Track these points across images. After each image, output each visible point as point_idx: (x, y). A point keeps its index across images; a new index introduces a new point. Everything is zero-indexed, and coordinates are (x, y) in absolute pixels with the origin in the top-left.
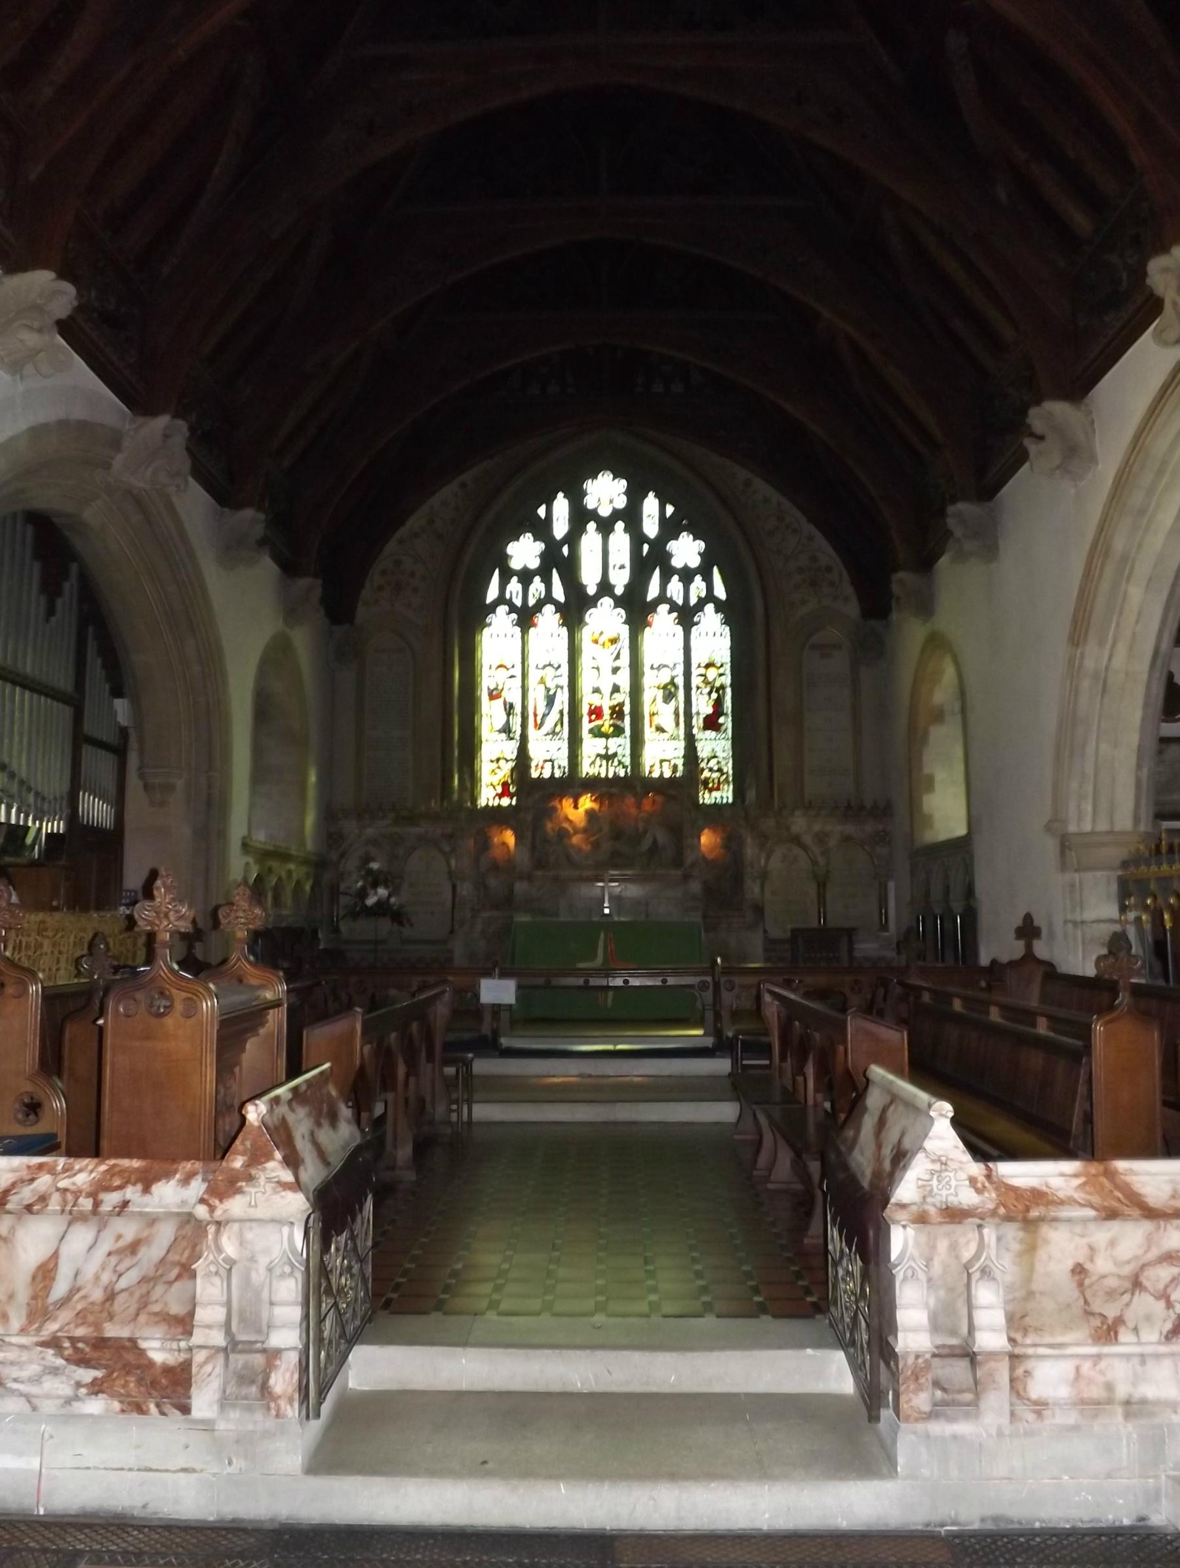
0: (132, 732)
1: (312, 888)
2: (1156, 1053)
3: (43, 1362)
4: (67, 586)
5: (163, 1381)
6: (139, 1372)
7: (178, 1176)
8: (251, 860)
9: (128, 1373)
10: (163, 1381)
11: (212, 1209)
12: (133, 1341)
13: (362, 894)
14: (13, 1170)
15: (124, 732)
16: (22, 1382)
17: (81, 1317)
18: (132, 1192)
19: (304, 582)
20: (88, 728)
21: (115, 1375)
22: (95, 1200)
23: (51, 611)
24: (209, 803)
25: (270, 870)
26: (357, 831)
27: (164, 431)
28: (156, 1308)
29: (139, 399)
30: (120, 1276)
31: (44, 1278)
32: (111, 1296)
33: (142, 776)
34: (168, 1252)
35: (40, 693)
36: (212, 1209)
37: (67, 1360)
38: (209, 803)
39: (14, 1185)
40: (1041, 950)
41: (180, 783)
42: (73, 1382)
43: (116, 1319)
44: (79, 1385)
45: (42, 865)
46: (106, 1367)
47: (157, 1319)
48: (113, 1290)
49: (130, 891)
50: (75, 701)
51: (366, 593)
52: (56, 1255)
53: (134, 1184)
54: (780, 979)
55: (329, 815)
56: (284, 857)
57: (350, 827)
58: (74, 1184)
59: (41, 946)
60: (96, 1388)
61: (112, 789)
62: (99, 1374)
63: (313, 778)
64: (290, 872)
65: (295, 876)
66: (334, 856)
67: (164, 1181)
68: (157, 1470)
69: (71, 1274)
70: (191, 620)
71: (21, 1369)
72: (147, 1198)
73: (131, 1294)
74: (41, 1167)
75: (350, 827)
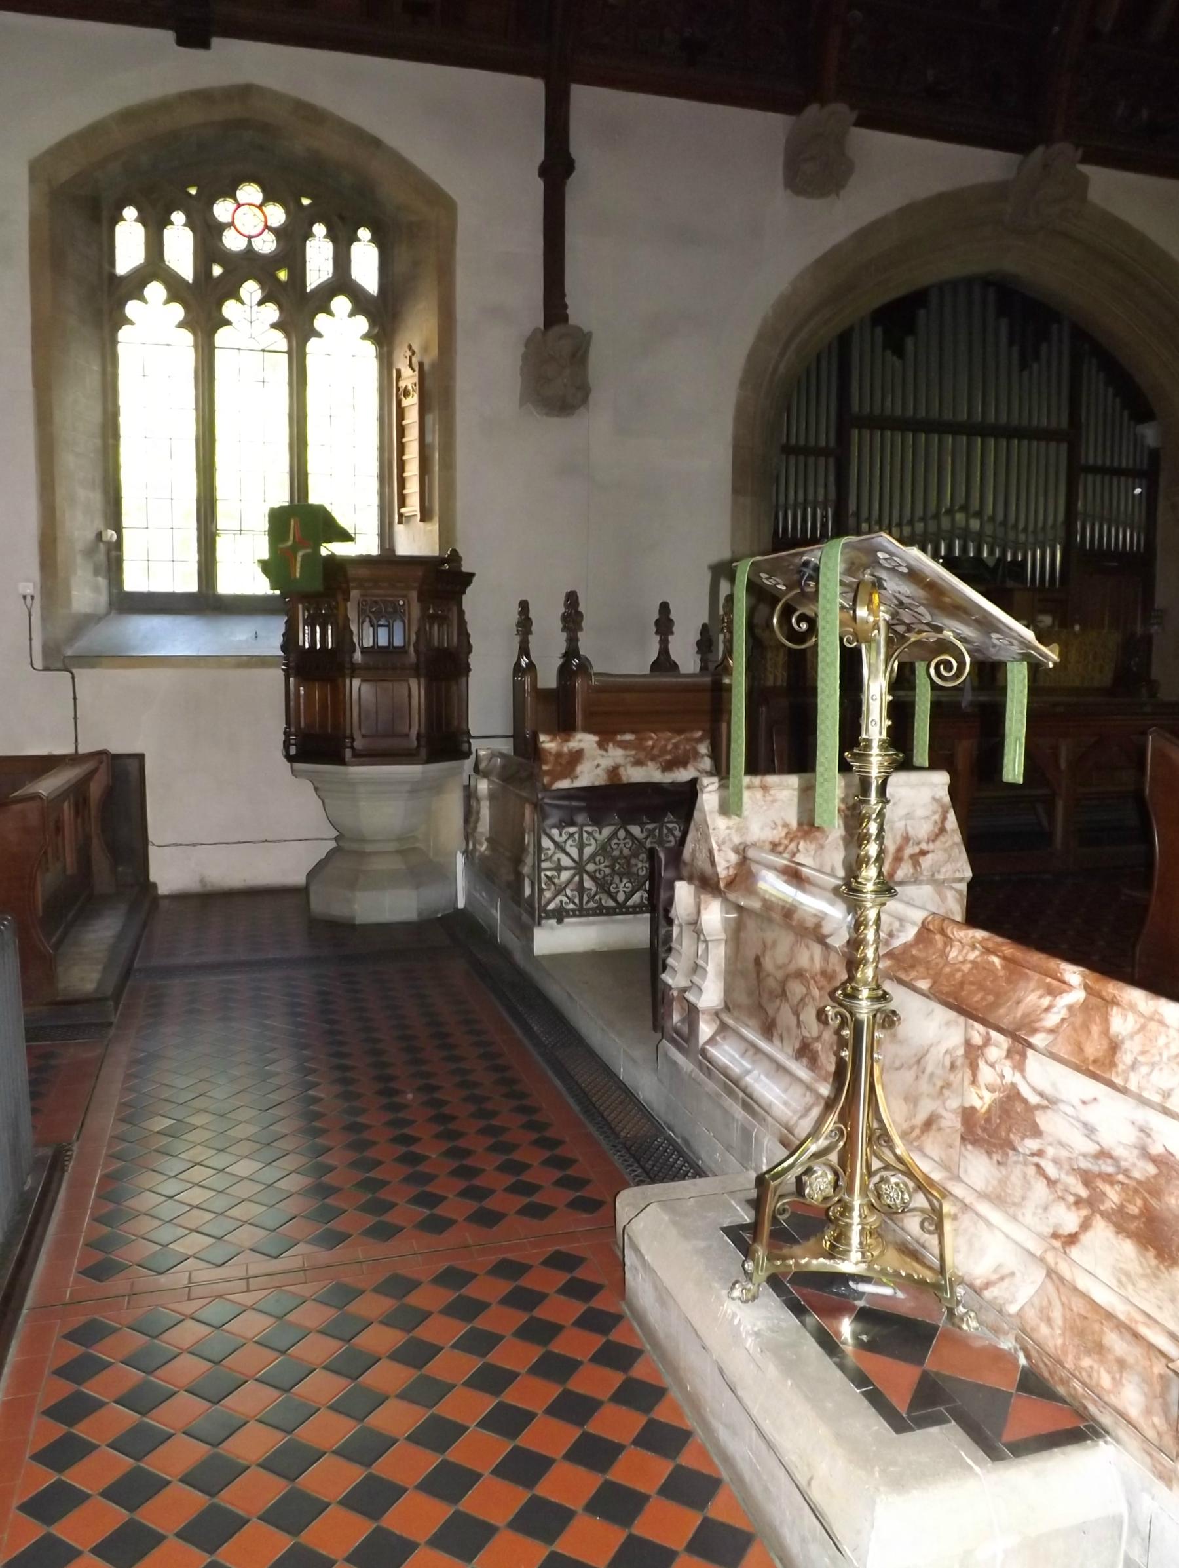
50: (1071, 436)
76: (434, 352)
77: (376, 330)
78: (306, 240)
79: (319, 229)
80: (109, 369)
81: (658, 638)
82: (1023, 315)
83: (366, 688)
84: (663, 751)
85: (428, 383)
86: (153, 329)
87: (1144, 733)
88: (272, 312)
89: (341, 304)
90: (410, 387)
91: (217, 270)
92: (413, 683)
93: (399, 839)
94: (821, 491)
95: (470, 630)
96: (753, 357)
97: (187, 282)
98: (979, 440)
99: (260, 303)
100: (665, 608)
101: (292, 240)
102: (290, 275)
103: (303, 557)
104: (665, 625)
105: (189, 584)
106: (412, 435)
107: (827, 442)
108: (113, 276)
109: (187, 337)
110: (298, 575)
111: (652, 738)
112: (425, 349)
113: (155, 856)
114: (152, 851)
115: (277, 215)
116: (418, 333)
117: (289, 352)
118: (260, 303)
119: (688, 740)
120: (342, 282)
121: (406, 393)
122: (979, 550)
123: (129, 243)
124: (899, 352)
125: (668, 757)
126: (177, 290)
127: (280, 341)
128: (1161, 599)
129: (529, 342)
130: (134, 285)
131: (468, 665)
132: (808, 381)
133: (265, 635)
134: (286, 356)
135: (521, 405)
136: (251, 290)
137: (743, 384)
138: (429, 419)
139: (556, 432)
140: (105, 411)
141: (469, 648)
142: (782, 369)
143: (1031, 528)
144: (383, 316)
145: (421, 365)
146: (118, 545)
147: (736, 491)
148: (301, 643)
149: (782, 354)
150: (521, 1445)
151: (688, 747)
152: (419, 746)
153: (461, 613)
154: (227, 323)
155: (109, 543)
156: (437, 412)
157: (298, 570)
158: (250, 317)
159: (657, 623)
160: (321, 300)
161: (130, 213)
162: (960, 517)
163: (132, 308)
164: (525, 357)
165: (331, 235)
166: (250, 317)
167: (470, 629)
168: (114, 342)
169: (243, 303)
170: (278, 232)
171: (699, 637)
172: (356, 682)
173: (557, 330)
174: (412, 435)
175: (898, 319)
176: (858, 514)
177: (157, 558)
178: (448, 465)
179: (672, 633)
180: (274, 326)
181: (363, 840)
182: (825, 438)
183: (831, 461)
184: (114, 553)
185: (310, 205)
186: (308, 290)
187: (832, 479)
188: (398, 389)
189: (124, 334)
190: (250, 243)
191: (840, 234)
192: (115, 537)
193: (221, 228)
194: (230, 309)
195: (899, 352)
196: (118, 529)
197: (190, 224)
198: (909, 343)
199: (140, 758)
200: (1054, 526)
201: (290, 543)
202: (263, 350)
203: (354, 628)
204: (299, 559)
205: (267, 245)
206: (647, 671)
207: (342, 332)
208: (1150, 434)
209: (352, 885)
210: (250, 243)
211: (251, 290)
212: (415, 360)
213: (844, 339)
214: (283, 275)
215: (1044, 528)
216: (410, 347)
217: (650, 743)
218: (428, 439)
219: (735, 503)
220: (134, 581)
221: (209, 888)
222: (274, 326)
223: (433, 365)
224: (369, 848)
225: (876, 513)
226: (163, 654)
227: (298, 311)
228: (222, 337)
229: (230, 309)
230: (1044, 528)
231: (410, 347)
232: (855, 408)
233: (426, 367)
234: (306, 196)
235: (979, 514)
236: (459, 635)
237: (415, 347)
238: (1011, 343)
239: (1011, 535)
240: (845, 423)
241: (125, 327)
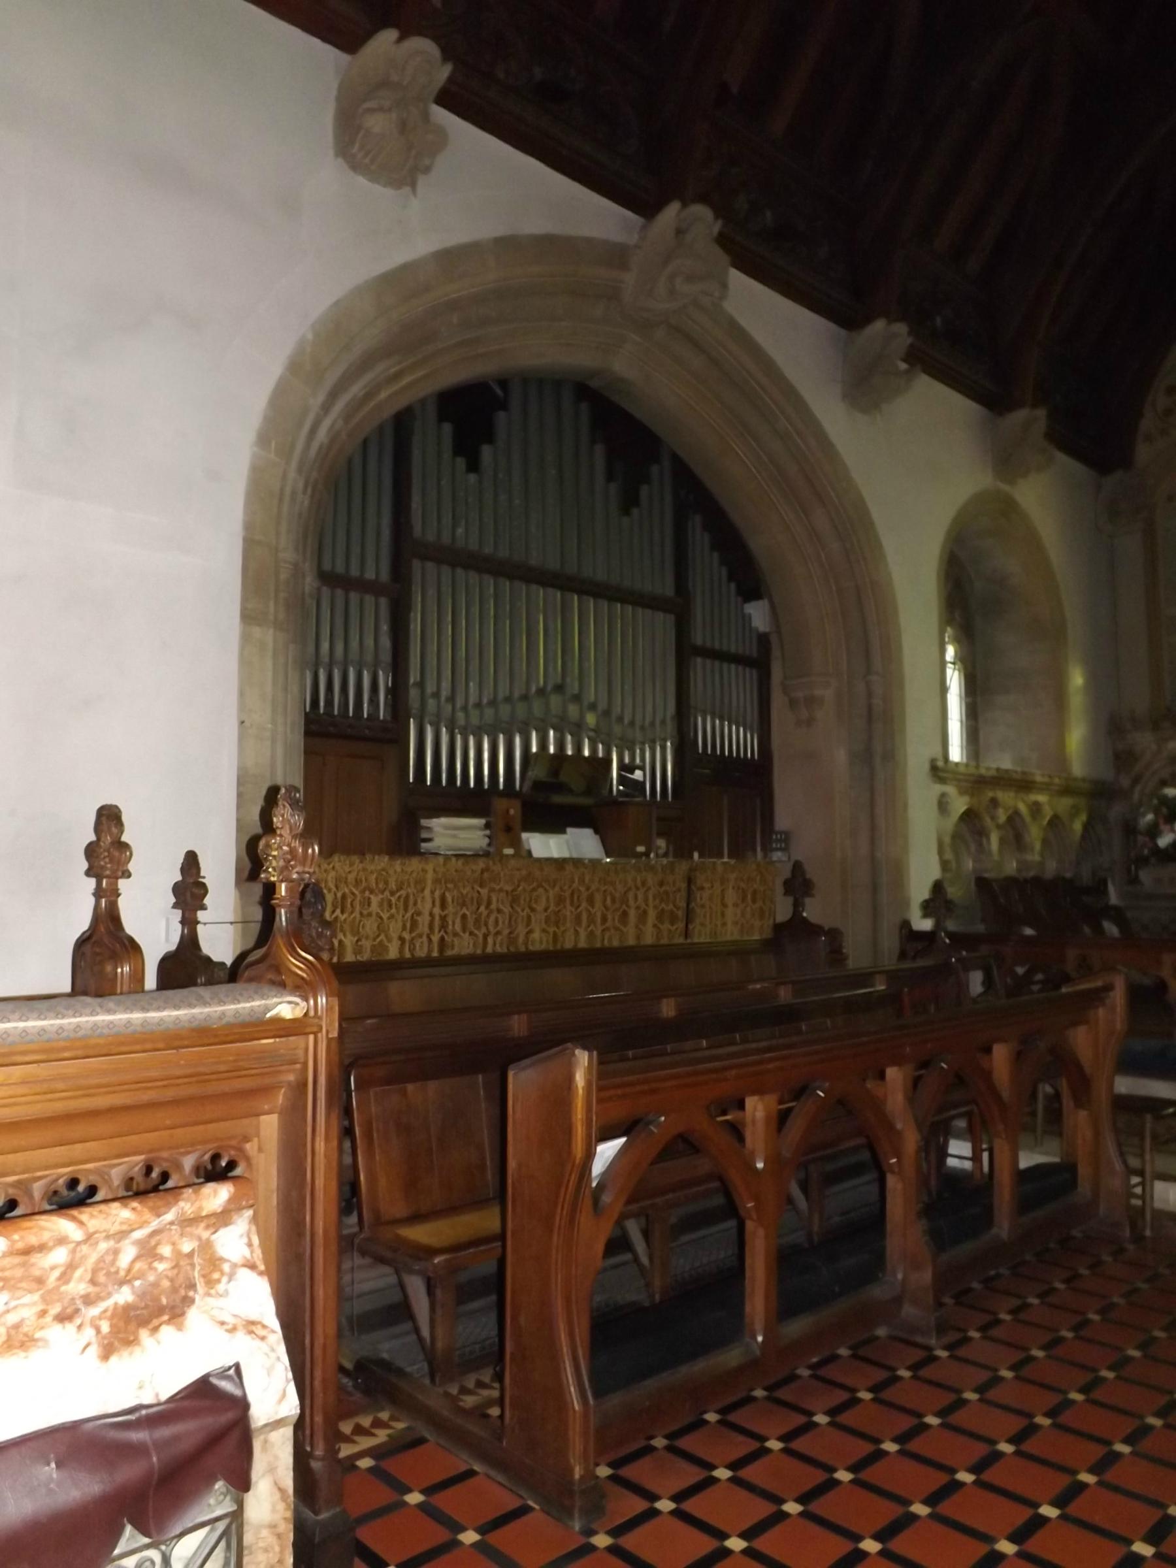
0: (774, 640)
1: (1087, 827)
4: (655, 469)
8: (950, 790)
13: (1153, 832)
15: (763, 640)
19: (1020, 416)
20: (698, 638)
23: (629, 502)
24: (870, 718)
25: (994, 802)
26: (1154, 747)
27: (691, 222)
29: (638, 190)
33: (785, 690)
35: (612, 599)
38: (870, 718)
40: (812, 912)
41: (828, 694)
49: (781, 833)
50: (679, 608)
51: (1147, 423)
55: (1114, 727)
56: (1024, 785)
57: (1144, 741)
59: (381, 904)
61: (752, 714)
63: (1077, 679)
64: (1036, 809)
65: (1048, 813)
66: (1125, 782)
70: (815, 482)
75: (1144, 741)
81: (92, 883)
82: (621, 436)
84: (105, 1276)
87: (988, 1050)
94: (369, 642)
96: (280, 393)
98: (576, 597)
100: (109, 817)
104: (107, 852)
107: (377, 574)
111: (62, 1241)
119: (187, 1222)
122: (578, 748)
124: (474, 466)
125: (125, 1296)
128: (782, 821)
132: (350, 479)
137: (263, 439)
142: (322, 435)
143: (638, 723)
147: (247, 617)
149: (326, 408)
151: (187, 1246)
159: (91, 851)
162: (555, 700)
171: (178, 877)
175: (471, 412)
176: (421, 685)
179: (127, 875)
182: (378, 569)
183: (383, 601)
187: (385, 628)
191: (420, 246)
195: (474, 466)
198: (486, 452)
200: (663, 722)
206: (58, 976)
208: (758, 615)
213: (402, 424)
215: (653, 724)
217: (59, 1256)
219: (245, 638)
225: (446, 686)
230: (653, 724)
232: (417, 530)
235: (577, 698)
238: (610, 477)
239: (617, 730)
240: (404, 548)
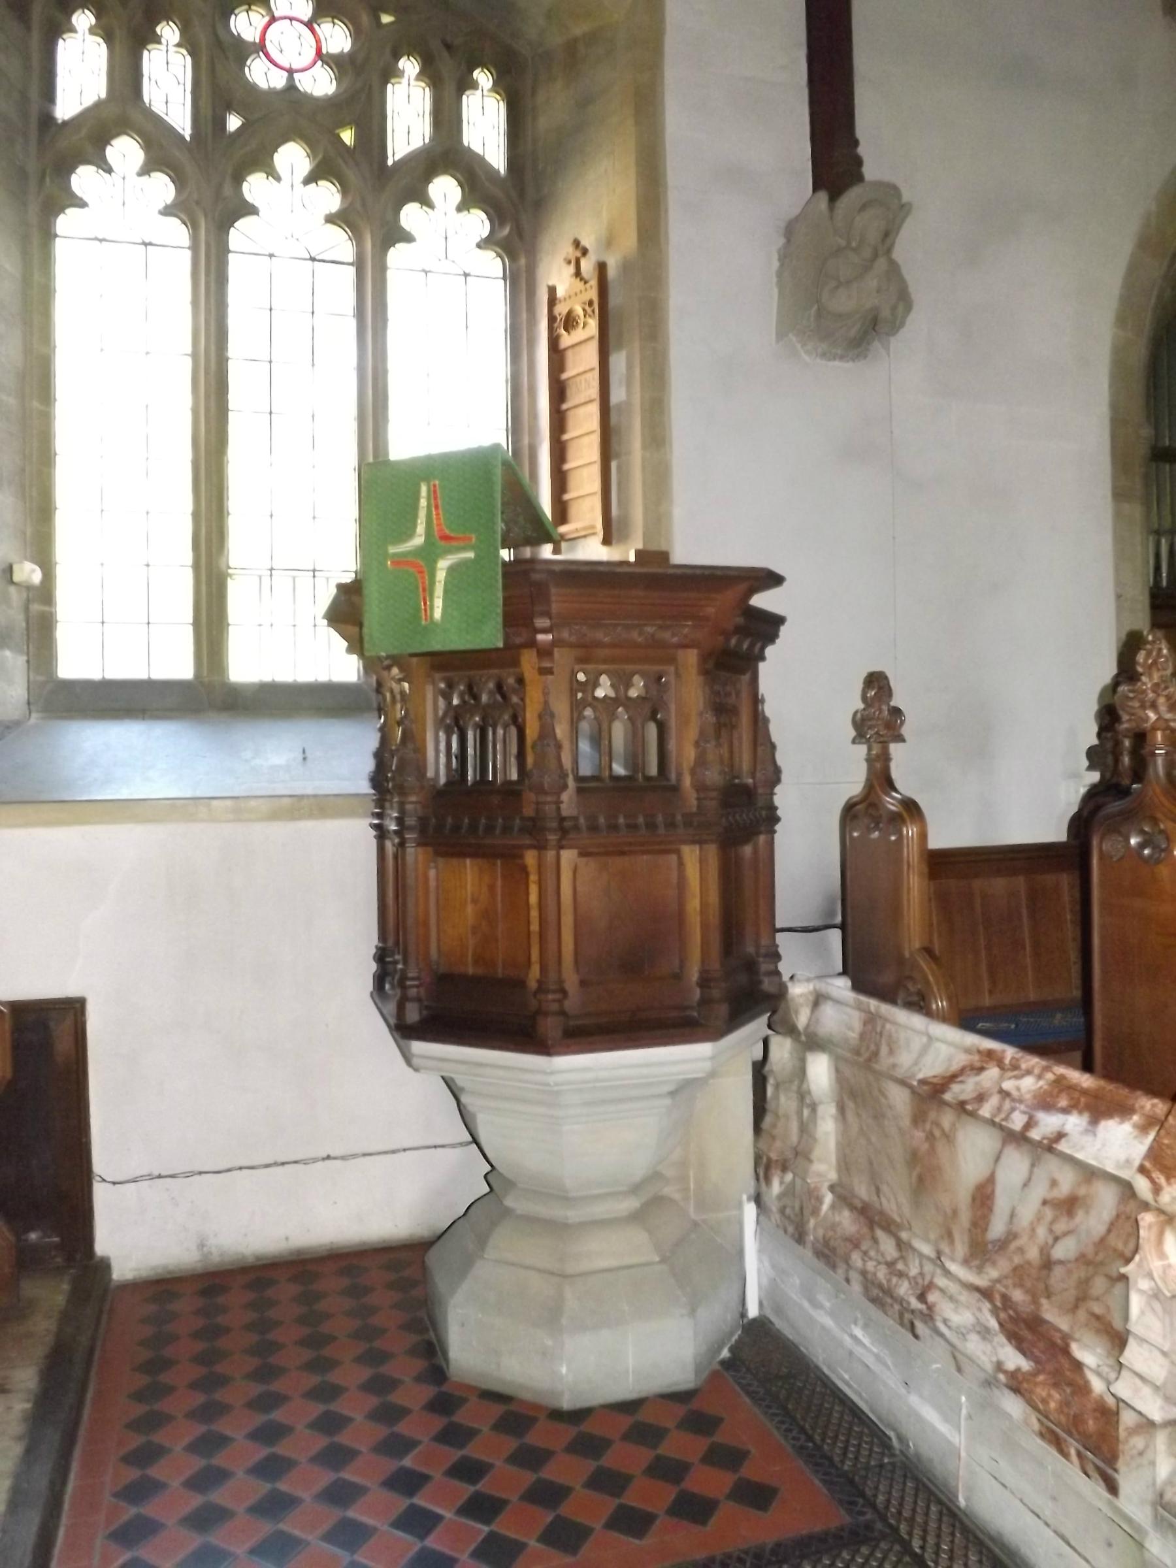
2: (472, 1523)
3: (978, 1314)
5: (1091, 1422)
6: (1068, 1390)
7: (1136, 1118)
9: (1056, 1385)
10: (1091, 1422)
11: (1157, 1190)
12: (1066, 1338)
14: (968, 1051)
16: (949, 1328)
17: (1019, 1273)
18: (1074, 1123)
21: (1041, 1378)
22: (1031, 1118)
28: (1097, 1309)
30: (1056, 1239)
31: (983, 1204)
32: (1048, 1264)
34: (1109, 1231)
36: (1157, 1190)
37: (1001, 1324)
39: (962, 1071)
42: (994, 1359)
43: (1053, 1299)
44: (999, 1367)
45: (571, 682)
46: (1037, 1361)
47: (1096, 1324)
48: (1049, 1256)
52: (991, 1180)
53: (1081, 1112)
54: (715, 965)
58: (1018, 1089)
60: (1017, 1384)
62: (1025, 1365)
67: (1117, 1119)
68: (1079, 1554)
69: (1007, 1212)
71: (956, 1310)
72: (1089, 1139)
73: (1069, 1272)
74: (990, 1055)
76: (629, 241)
77: (506, 231)
78: (386, 82)
79: (409, 66)
80: (37, 277)
83: (589, 867)
85: (614, 300)
86: (119, 211)
88: (328, 196)
89: (445, 189)
90: (579, 311)
91: (234, 123)
92: (691, 854)
93: (635, 1189)
95: (775, 736)
97: (182, 137)
99: (308, 180)
101: (363, 78)
102: (358, 137)
103: (451, 570)
105: (177, 663)
106: (584, 390)
108: (47, 120)
109: (177, 232)
110: (438, 614)
112: (609, 242)
113: (105, 1202)
114: (100, 1193)
115: (337, 37)
116: (591, 215)
117: (359, 264)
118: (308, 180)
120: (446, 152)
121: (570, 322)
123: (81, 68)
126: (161, 151)
127: (340, 244)
129: (790, 230)
130: (92, 137)
131: (773, 808)
133: (345, 758)
134: (352, 270)
135: (781, 335)
136: (293, 158)
138: (618, 361)
139: (839, 389)
140: (27, 350)
141: (776, 776)
144: (515, 208)
145: (602, 267)
146: (45, 593)
147: (1119, 495)
148: (430, 774)
150: (465, 1485)
152: (705, 1002)
153: (756, 700)
154: (252, 210)
155: (29, 588)
156: (637, 345)
157: (438, 603)
158: (290, 201)
160: (412, 179)
161: (83, 20)
163: (84, 179)
164: (784, 256)
165: (430, 74)
166: (290, 201)
167: (776, 733)
168: (48, 235)
169: (278, 179)
170: (337, 63)
172: (568, 856)
173: (852, 196)
174: (584, 390)
177: (117, 609)
178: (657, 438)
180: (331, 219)
181: (565, 1198)
184: (36, 607)
185: (392, 23)
186: (390, 162)
188: (552, 319)
189: (67, 222)
190: (291, 78)
192: (37, 577)
193: (242, 51)
194: (255, 187)
196: (44, 558)
197: (188, 42)
199: (72, 1010)
201: (418, 540)
202: (313, 259)
203: (561, 731)
204: (441, 576)
205: (320, 83)
207: (445, 231)
209: (552, 1317)
210: (291, 78)
211: (293, 158)
212: (587, 266)
214: (347, 136)
216: (577, 244)
218: (618, 395)
219: (1118, 515)
220: (75, 662)
221: (216, 1258)
222: (331, 219)
223: (626, 267)
224: (573, 1215)
226: (124, 794)
227: (375, 196)
228: (241, 234)
229: (255, 187)
231: (577, 244)
233: (612, 272)
234: (387, 12)
236: (755, 744)
237: (585, 242)
241: (69, 211)
